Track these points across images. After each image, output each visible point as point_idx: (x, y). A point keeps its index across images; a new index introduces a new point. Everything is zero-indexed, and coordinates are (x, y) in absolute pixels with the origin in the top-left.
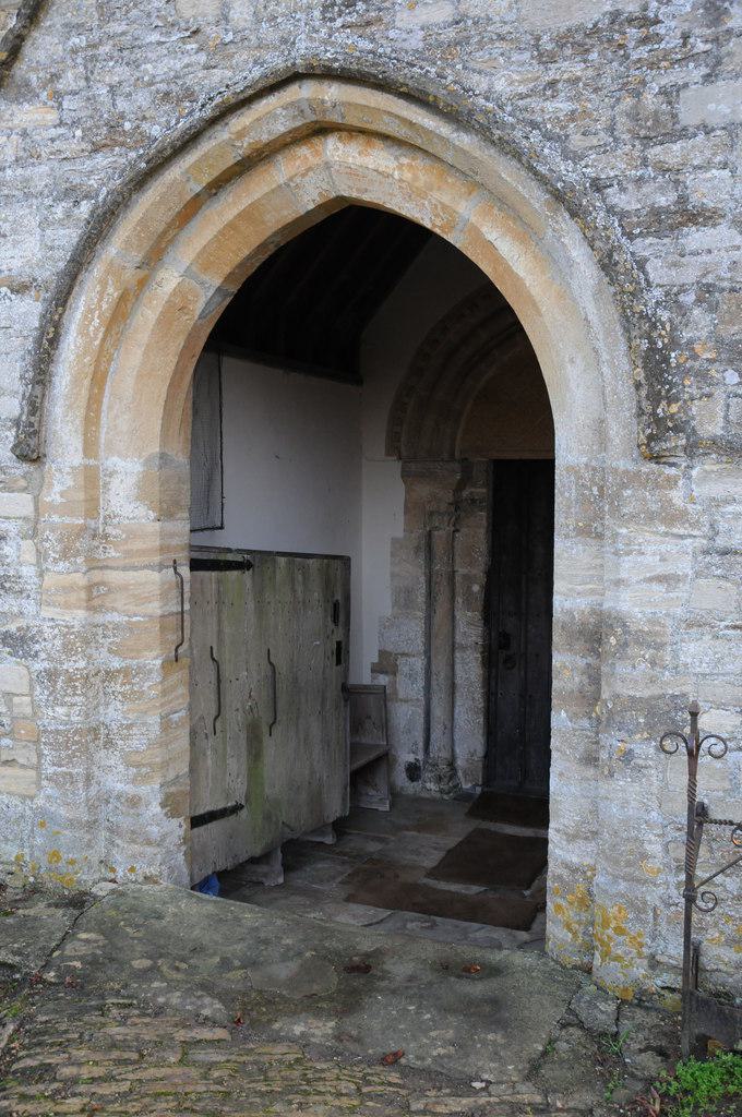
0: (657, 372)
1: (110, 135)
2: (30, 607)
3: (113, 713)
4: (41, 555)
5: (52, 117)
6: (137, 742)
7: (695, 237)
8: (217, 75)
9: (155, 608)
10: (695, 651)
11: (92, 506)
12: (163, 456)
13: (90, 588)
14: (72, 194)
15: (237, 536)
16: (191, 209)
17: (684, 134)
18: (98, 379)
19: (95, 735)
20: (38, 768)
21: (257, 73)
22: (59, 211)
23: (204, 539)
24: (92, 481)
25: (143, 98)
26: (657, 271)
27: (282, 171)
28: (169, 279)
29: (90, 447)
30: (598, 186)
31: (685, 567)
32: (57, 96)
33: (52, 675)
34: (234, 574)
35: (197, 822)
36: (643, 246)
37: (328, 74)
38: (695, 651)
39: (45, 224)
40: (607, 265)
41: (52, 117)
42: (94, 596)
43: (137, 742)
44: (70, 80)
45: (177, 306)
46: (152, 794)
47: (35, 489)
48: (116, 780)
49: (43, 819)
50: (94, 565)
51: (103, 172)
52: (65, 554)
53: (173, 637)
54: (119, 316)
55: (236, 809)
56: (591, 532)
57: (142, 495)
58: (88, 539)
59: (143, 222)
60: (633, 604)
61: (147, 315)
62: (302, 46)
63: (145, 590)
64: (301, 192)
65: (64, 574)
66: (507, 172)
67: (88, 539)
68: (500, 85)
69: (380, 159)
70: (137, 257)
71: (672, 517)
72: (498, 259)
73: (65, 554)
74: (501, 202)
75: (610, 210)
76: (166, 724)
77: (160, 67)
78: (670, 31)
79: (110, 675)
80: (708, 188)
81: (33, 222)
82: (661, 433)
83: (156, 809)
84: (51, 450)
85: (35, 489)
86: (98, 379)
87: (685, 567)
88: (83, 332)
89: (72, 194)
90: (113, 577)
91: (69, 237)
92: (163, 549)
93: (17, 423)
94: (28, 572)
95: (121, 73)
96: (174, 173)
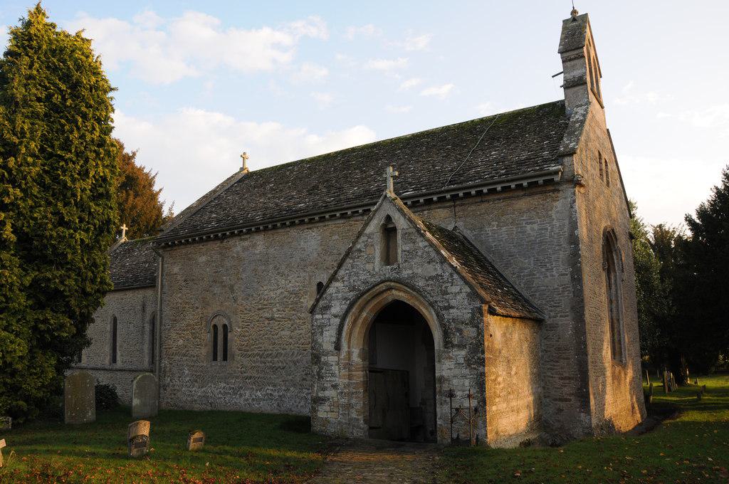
0: (446, 334)
1: (353, 289)
2: (337, 379)
3: (353, 401)
4: (339, 369)
5: (342, 285)
6: (358, 407)
7: (451, 311)
8: (372, 279)
9: (362, 379)
10: (455, 381)
11: (349, 359)
12: (363, 349)
13: (349, 375)
14: (346, 299)
15: (380, 365)
16: (368, 302)
17: (449, 294)
18: (351, 334)
19: (349, 406)
20: (339, 412)
21: (379, 280)
22: (343, 302)
23: (372, 366)
24: (349, 353)
25: (359, 283)
26: (446, 316)
27: (385, 295)
28: (364, 314)
29: (349, 347)
30: (436, 302)
31: (453, 367)
32: (343, 281)
33: (342, 393)
34: (379, 374)
35: (371, 428)
36: (444, 312)
37: (391, 281)
38: (455, 381)
39: (341, 304)
40: (438, 316)
41: (342, 285)
42: (350, 377)
43: (358, 407)
44: (346, 278)
45: (366, 319)
46: (361, 417)
47: (338, 355)
48: (354, 415)
49: (340, 423)
50: (350, 370)
51: (351, 295)
52: (344, 368)
53: (365, 386)
54: (354, 322)
55: (380, 428)
56: (439, 361)
57: (359, 356)
58: (348, 366)
59: (359, 305)
60: (445, 374)
61: (360, 321)
62: (387, 276)
63: (359, 376)
64: (423, 452)
65: (344, 372)
66: (422, 299)
67: (348, 366)
68: (420, 284)
69: (401, 294)
70: (358, 311)
71: (450, 358)
72: (419, 308)
73: (344, 368)
74: (421, 303)
75: (438, 306)
76: (364, 403)
77: (362, 277)
78: (445, 278)
79: (353, 393)
80: (453, 302)
81: (338, 304)
82: (448, 344)
83: (362, 421)
84: (342, 348)
85: (338, 355)
86: (351, 334)
87: (453, 367)
88: (348, 325)
89: (346, 299)
90: (353, 373)
91: (345, 307)
92: (363, 367)
93: (335, 342)
94: (337, 372)
95: (355, 278)
96: (365, 296)
